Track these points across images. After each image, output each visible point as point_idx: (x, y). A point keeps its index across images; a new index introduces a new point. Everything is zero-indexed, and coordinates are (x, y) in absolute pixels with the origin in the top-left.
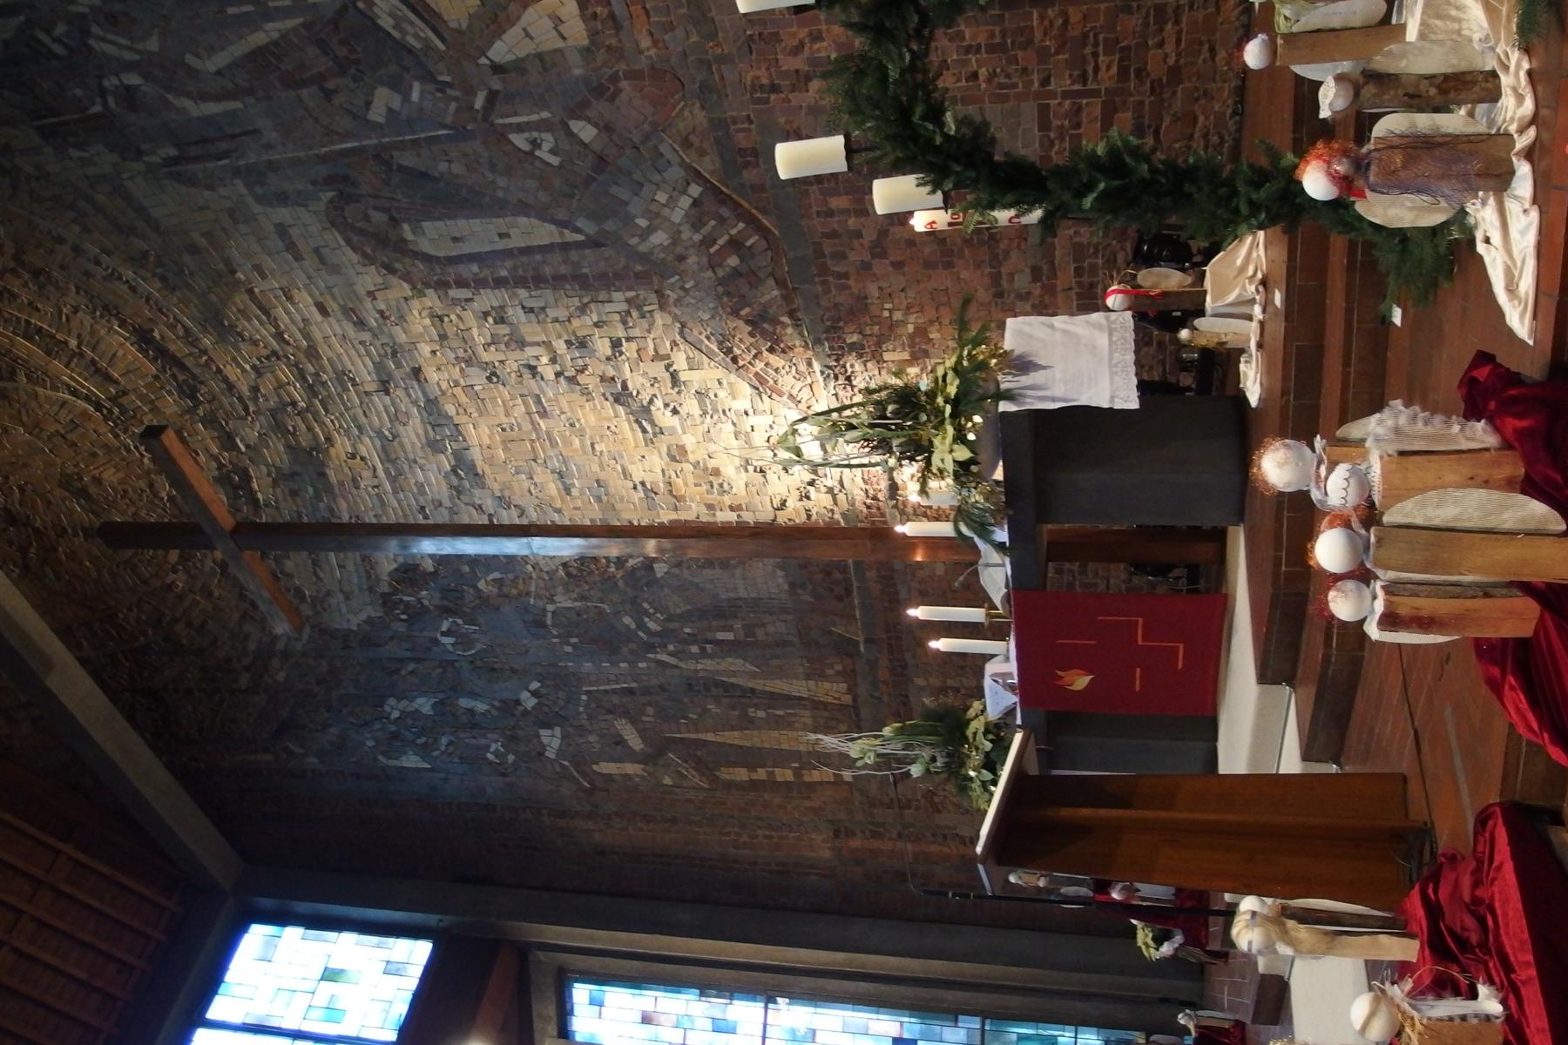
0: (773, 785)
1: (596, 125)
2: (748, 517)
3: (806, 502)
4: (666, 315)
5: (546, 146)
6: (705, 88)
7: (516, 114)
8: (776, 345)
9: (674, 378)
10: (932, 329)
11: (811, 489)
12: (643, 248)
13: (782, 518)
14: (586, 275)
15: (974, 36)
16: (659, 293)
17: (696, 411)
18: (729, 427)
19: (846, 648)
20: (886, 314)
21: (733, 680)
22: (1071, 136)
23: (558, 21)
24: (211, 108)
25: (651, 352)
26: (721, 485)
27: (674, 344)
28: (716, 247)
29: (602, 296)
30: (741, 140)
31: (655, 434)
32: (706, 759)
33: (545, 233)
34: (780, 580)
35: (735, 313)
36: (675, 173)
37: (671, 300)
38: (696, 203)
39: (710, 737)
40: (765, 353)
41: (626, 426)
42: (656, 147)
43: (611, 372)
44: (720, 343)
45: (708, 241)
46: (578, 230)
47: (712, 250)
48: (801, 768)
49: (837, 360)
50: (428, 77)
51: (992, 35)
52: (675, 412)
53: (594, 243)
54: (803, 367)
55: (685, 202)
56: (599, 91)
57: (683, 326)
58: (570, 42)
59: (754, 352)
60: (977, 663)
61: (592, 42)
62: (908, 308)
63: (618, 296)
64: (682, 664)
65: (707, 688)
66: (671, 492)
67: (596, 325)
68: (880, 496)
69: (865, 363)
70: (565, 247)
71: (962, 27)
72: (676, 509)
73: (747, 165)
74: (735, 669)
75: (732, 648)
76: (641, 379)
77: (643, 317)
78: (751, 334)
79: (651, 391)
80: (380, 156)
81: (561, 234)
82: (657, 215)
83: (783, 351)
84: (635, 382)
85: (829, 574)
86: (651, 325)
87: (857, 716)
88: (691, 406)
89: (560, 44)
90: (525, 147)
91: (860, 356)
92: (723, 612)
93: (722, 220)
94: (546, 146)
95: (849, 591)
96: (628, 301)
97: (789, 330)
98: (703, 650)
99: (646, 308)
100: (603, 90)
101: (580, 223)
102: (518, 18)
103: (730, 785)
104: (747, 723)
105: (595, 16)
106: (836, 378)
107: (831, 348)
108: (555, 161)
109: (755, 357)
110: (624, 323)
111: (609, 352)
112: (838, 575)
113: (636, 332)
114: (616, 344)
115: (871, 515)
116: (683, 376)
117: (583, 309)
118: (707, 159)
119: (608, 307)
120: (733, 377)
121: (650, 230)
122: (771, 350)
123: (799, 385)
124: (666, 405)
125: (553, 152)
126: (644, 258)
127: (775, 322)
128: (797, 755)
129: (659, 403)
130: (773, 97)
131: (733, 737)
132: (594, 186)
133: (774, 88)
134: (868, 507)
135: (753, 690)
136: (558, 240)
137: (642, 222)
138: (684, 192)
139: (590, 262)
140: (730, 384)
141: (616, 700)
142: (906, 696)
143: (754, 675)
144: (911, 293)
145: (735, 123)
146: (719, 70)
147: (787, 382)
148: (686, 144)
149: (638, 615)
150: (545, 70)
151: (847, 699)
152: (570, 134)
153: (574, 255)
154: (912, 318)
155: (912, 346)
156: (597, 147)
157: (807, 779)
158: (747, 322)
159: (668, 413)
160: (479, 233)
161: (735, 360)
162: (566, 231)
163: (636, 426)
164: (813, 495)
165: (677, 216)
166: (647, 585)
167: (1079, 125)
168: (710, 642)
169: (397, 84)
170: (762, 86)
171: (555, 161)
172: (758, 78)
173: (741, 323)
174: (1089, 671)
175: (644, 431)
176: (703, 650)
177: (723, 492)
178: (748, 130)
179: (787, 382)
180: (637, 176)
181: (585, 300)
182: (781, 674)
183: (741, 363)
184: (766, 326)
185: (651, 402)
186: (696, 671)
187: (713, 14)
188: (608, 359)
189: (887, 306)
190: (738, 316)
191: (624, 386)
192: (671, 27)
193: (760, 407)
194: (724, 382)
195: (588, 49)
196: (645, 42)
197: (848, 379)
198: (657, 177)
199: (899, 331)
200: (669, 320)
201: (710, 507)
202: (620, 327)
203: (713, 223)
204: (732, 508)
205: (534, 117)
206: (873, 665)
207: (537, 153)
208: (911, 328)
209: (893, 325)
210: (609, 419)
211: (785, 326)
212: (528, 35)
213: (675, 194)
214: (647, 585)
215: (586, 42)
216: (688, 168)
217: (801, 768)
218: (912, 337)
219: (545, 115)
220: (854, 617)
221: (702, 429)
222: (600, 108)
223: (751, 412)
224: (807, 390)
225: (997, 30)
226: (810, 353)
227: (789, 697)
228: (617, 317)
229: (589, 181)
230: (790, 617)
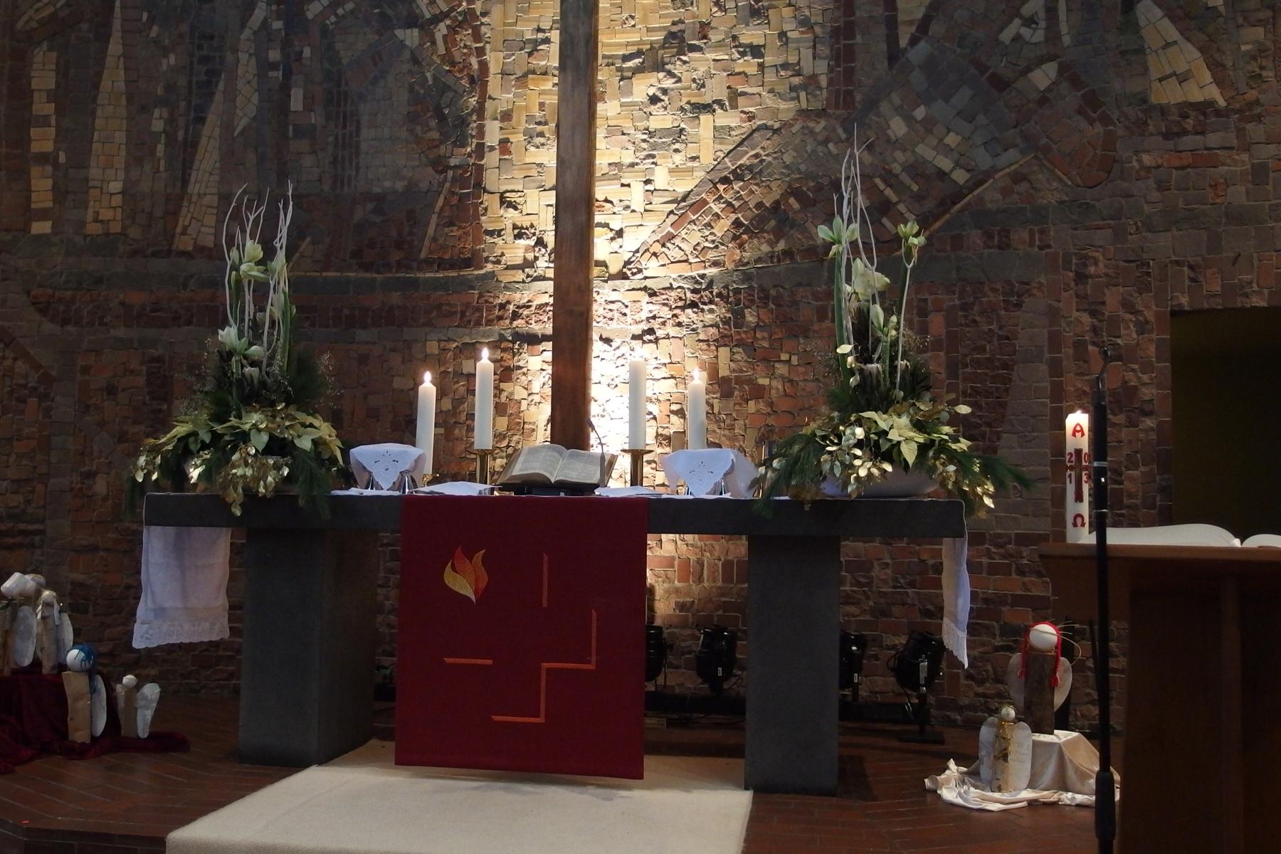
0: (22, 122)
1: (1049, 89)
2: (491, 159)
3: (509, 234)
4: (791, 115)
5: (1026, 32)
7: (1069, 10)
8: (740, 232)
9: (707, 108)
10: (762, 406)
11: (532, 242)
12: (884, 107)
13: (491, 201)
14: (853, 37)
15: (1131, 479)
16: (821, 113)
17: (654, 124)
18: (628, 158)
20: (784, 357)
21: (218, 97)
22: (1009, 566)
23: (1183, 78)
25: (740, 89)
26: (541, 134)
27: (751, 117)
28: (882, 186)
29: (823, 50)
30: (1020, 235)
31: (620, 69)
34: (387, 184)
35: (793, 192)
36: (983, 160)
37: (811, 124)
38: (942, 175)
39: (115, 47)
40: (733, 216)
41: (635, 38)
42: (1016, 146)
43: (714, 37)
44: (750, 168)
45: (889, 177)
46: (914, 41)
47: (878, 181)
48: (56, 165)
49: (719, 295)
51: (1130, 496)
52: (654, 100)
53: (894, 55)
54: (711, 255)
55: (945, 164)
57: (776, 131)
58: (1156, 85)
59: (737, 204)
60: (404, 430)
61: (1153, 107)
62: (791, 381)
63: (822, 67)
64: (247, 33)
65: (205, 60)
66: (534, 72)
67: (782, 35)
68: (519, 322)
69: (715, 325)
70: (892, 24)
71: (1142, 469)
72: (504, 73)
73: (990, 236)
75: (277, 103)
76: (702, 69)
77: (792, 89)
78: (759, 205)
79: (686, 77)
81: (911, 23)
82: (929, 131)
83: (735, 238)
84: (700, 63)
85: (399, 245)
86: (780, 96)
87: (154, 254)
88: (662, 119)
89: (1154, 74)
90: (1026, 10)
91: (726, 322)
92: (337, 100)
93: (919, 198)
94: (1026, 32)
95: (367, 267)
96: (813, 78)
97: (765, 248)
98: (274, 66)
99: (803, 95)
100: (1092, 104)
101: (923, 46)
102: (1188, 39)
104: (139, 104)
105: (1185, 116)
106: (694, 291)
107: (737, 291)
108: (1006, 36)
109: (729, 204)
110: (785, 66)
111: (744, 40)
112: (395, 256)
113: (770, 77)
114: (756, 51)
115: (490, 310)
116: (705, 118)
117: (805, 23)
118: (999, 196)
119: (807, 54)
120: (700, 174)
121: (908, 119)
122: (737, 223)
123: (688, 248)
124: (665, 91)
125: (1017, 38)
126: (872, 104)
127: (778, 234)
128: (80, 159)
129: (669, 83)
130: (1071, 275)
131: (114, 80)
132: (973, 71)
133: (1081, 278)
134: (503, 306)
135: (201, 120)
136: (901, 17)
137: (920, 113)
138: (957, 165)
139: (871, 45)
140: (692, 170)
142: (189, 323)
143: (228, 127)
144: (811, 386)
145: (1042, 232)
146: (1109, 226)
147: (692, 236)
148: (1018, 178)
150: (1123, 53)
151: (184, 243)
152: (1041, 61)
153: (882, 30)
154: (777, 384)
155: (739, 381)
156: (1018, 85)
157: (35, 171)
158: (777, 203)
159: (651, 91)
161: (725, 180)
162: (913, 29)
163: (633, 49)
164: (522, 242)
165: (925, 151)
166: (383, 15)
167: (1021, 572)
168: (288, 74)
170: (1086, 266)
171: (1006, 36)
172: (1096, 263)
173: (776, 195)
174: (483, 595)
175: (626, 58)
176: (274, 66)
177: (530, 136)
178: (1032, 244)
179: (692, 236)
180: (981, 119)
181: (818, 30)
183: (721, 187)
184: (773, 223)
185: (671, 74)
186: (235, 51)
187: (1175, 232)
188: (735, 38)
189: (795, 360)
190: (786, 195)
191: (694, 48)
192: (1162, 186)
193: (657, 200)
194: (696, 164)
195: (1144, 101)
196: (1147, 159)
197: (693, 305)
198: (979, 140)
199: (761, 368)
200: (786, 117)
201: (506, 116)
202: (780, 61)
203: (915, 188)
204: (504, 143)
205: (1064, 28)
207: (1017, 21)
208: (764, 381)
209: (768, 360)
210: (645, 19)
211: (772, 244)
212: (1168, 45)
213: (956, 156)
214: (383, 15)
215: (1154, 100)
216: (988, 174)
217: (56, 165)
218: (751, 382)
219: (1067, 40)
220: (326, 268)
221: (627, 125)
223: (650, 187)
224: (678, 255)
225: (1138, 502)
226: (730, 266)
227: (187, 165)
228: (793, 59)
229: (982, 68)
230: (326, 187)
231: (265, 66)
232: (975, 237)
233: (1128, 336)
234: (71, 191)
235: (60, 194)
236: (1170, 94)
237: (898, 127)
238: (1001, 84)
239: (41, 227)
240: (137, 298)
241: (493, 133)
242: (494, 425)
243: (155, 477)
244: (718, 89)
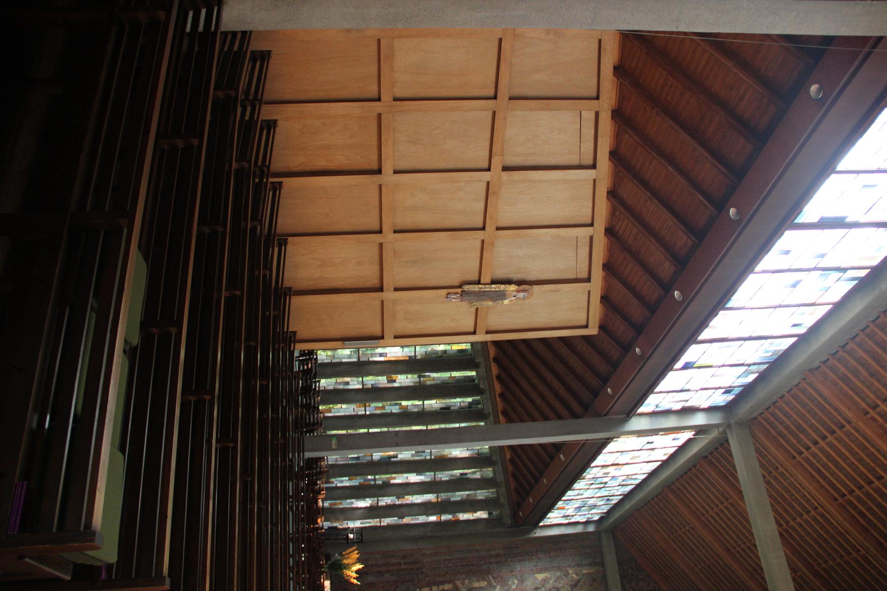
103: (449, 582)
243: (351, 536)
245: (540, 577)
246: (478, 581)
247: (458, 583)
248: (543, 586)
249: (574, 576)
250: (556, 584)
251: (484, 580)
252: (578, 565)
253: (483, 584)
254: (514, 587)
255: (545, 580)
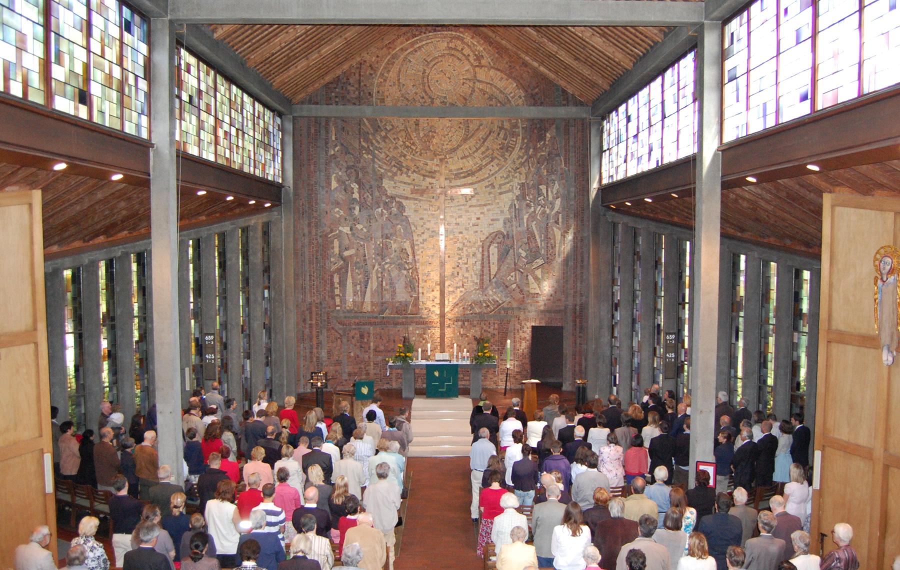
6: (520, 309)
19: (382, 312)
24: (525, 221)
30: (510, 312)
32: (342, 272)
33: (493, 272)
39: (349, 274)
50: (527, 263)
56: (521, 291)
74: (373, 284)
80: (512, 247)
103: (332, 276)
128: (344, 295)
131: (349, 281)
139: (486, 278)
141: (362, 251)
149: (391, 264)
160: (494, 258)
169: (526, 257)
182: (372, 295)
206: (376, 317)
222: (518, 290)
231: (378, 278)
232: (502, 312)
233: (525, 329)
234: (343, 300)
235: (341, 301)
236: (532, 291)
237: (491, 293)
238: (507, 287)
239: (338, 308)
240: (357, 321)
241: (421, 290)
242: (717, 397)
244: (460, 284)
245: (334, 184)
246: (333, 248)
247: (333, 268)
248: (344, 183)
249: (337, 149)
250: (344, 169)
251: (332, 242)
252: (327, 143)
253: (336, 243)
254: (342, 213)
255: (339, 180)
